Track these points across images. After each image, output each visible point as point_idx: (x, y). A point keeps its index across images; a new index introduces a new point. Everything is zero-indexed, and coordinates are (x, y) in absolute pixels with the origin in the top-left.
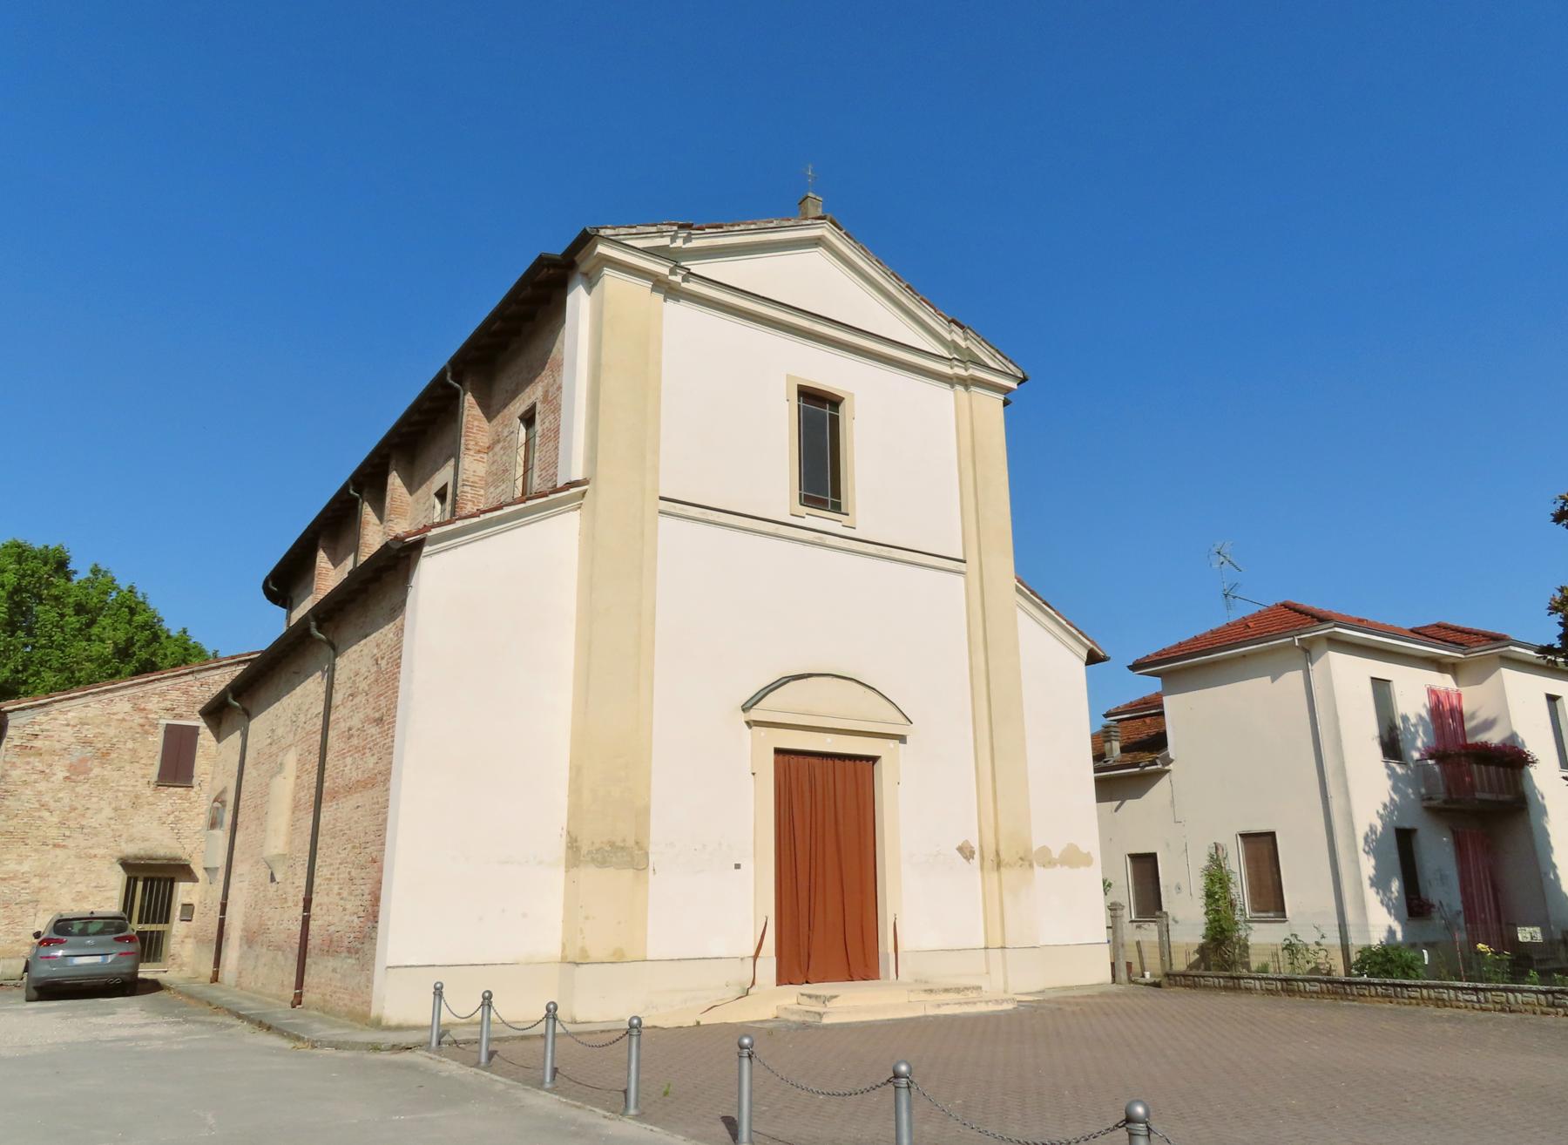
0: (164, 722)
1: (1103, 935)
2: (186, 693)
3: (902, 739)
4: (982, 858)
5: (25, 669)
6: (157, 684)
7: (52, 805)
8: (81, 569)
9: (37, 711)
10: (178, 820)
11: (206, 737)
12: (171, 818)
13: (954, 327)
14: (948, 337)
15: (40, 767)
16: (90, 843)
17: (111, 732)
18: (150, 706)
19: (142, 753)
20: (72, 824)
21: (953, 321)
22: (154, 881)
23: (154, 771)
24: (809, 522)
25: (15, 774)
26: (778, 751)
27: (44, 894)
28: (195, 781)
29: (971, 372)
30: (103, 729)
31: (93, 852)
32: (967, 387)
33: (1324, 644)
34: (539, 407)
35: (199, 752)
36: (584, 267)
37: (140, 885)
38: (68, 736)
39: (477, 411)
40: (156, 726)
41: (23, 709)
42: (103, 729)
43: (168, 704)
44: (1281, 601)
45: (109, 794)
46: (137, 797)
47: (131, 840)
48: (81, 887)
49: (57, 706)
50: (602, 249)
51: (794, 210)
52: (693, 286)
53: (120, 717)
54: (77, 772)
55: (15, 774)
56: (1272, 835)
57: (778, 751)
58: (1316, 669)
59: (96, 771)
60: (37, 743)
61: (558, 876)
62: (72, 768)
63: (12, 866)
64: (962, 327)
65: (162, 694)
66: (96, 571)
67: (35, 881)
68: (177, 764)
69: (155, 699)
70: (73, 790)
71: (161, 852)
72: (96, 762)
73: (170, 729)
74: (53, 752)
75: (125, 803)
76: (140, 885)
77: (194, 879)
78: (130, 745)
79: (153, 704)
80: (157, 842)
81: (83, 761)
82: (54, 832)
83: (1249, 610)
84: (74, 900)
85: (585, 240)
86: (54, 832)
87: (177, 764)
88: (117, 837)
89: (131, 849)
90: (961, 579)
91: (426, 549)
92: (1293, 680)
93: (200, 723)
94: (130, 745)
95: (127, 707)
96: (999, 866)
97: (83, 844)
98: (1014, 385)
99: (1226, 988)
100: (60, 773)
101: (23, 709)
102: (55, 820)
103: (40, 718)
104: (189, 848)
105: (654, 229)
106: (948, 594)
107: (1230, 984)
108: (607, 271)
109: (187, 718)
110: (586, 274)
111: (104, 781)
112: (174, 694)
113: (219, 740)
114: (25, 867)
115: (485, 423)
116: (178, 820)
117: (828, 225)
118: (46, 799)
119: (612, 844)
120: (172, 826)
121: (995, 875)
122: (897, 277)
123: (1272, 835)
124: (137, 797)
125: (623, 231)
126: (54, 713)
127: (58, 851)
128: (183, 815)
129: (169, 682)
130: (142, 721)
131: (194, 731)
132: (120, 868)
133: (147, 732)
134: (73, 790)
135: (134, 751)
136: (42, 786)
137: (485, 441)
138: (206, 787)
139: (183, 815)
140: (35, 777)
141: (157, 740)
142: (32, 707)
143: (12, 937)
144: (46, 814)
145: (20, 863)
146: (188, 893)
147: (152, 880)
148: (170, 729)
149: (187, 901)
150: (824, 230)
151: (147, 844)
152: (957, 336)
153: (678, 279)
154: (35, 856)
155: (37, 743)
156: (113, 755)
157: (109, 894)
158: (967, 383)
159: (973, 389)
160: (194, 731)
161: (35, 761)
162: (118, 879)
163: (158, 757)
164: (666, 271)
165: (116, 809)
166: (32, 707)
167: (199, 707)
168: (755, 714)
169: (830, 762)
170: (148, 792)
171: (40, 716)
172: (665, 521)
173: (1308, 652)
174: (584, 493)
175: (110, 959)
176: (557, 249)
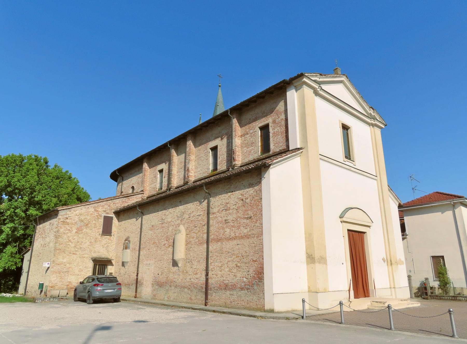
0: (103, 215)
1: (407, 284)
2: (109, 206)
3: (369, 227)
4: (387, 262)
5: (45, 196)
6: (101, 203)
7: (72, 240)
8: (51, 165)
9: (67, 210)
10: (108, 246)
11: (115, 220)
12: (106, 246)
13: (371, 109)
14: (369, 112)
15: (69, 228)
16: (83, 253)
17: (89, 218)
18: (99, 210)
19: (97, 225)
20: (78, 247)
21: (371, 107)
22: (101, 264)
23: (101, 230)
24: (347, 163)
25: (61, 230)
26: (348, 230)
27: (70, 269)
28: (112, 234)
29: (376, 122)
30: (86, 217)
31: (84, 256)
32: (373, 127)
33: (460, 204)
34: (270, 125)
35: (113, 225)
36: (295, 84)
37: (97, 266)
38: (76, 219)
39: (237, 124)
40: (101, 216)
41: (64, 210)
42: (86, 217)
43: (104, 209)
44: (435, 191)
45: (88, 238)
46: (96, 239)
47: (95, 252)
48: (81, 267)
49: (73, 209)
50: (305, 79)
51: (335, 72)
52: (321, 92)
53: (91, 213)
54: (79, 230)
55: (61, 230)
56: (443, 257)
57: (348, 230)
58: (457, 211)
59: (85, 230)
60: (68, 221)
61: (303, 267)
62: (78, 229)
63: (61, 260)
64: (373, 109)
65: (103, 206)
66: (56, 166)
67: (68, 265)
68: (107, 230)
69: (101, 208)
70: (78, 236)
71: (103, 256)
72: (84, 227)
73: (105, 217)
74: (72, 224)
75: (93, 241)
76: (97, 266)
77: (112, 265)
78: (94, 222)
79: (100, 209)
80: (103, 253)
81: (81, 227)
82: (73, 249)
83: (422, 195)
84: (79, 271)
85: (301, 76)
86: (73, 249)
87: (107, 230)
88: (91, 251)
89: (95, 255)
90: (375, 181)
91: (271, 166)
92: (449, 213)
93: (113, 216)
94: (94, 222)
95: (93, 210)
96: (391, 264)
97: (81, 253)
98: (383, 127)
99: (452, 300)
100: (75, 231)
101: (64, 210)
102: (73, 245)
103: (68, 213)
104: (111, 255)
105: (315, 75)
106: (372, 185)
107: (453, 298)
108: (304, 86)
109: (110, 214)
110: (295, 86)
111: (87, 233)
112: (106, 206)
113: (119, 221)
114: (65, 261)
115: (240, 128)
116: (108, 246)
117: (345, 77)
118: (71, 238)
119: (321, 257)
120: (107, 248)
121: (390, 267)
122: (359, 93)
123: (443, 257)
124: (96, 239)
125: (309, 74)
126: (72, 211)
127: (74, 255)
128: (109, 245)
129: (105, 202)
130: (97, 214)
131: (112, 218)
132: (92, 261)
133: (98, 218)
134: (78, 236)
135: (95, 224)
136: (69, 234)
137: (240, 134)
138: (115, 236)
139: (109, 245)
140: (67, 231)
141: (101, 220)
142: (66, 209)
143: (61, 283)
144: (70, 243)
145: (63, 259)
146: (111, 269)
147: (101, 265)
148: (105, 217)
149: (111, 272)
150: (343, 78)
151: (99, 254)
152: (371, 111)
153: (319, 90)
154: (68, 257)
155: (68, 221)
156: (89, 225)
157: (89, 269)
158: (373, 125)
159: (375, 127)
160: (112, 218)
161: (67, 226)
162: (91, 265)
163: (102, 226)
164: (317, 87)
165: (90, 242)
166: (66, 209)
167: (113, 211)
168: (344, 219)
169: (358, 233)
170: (99, 237)
171: (68, 212)
172: (321, 161)
173: (454, 206)
174: (302, 152)
175: (116, 290)
176: (288, 79)
